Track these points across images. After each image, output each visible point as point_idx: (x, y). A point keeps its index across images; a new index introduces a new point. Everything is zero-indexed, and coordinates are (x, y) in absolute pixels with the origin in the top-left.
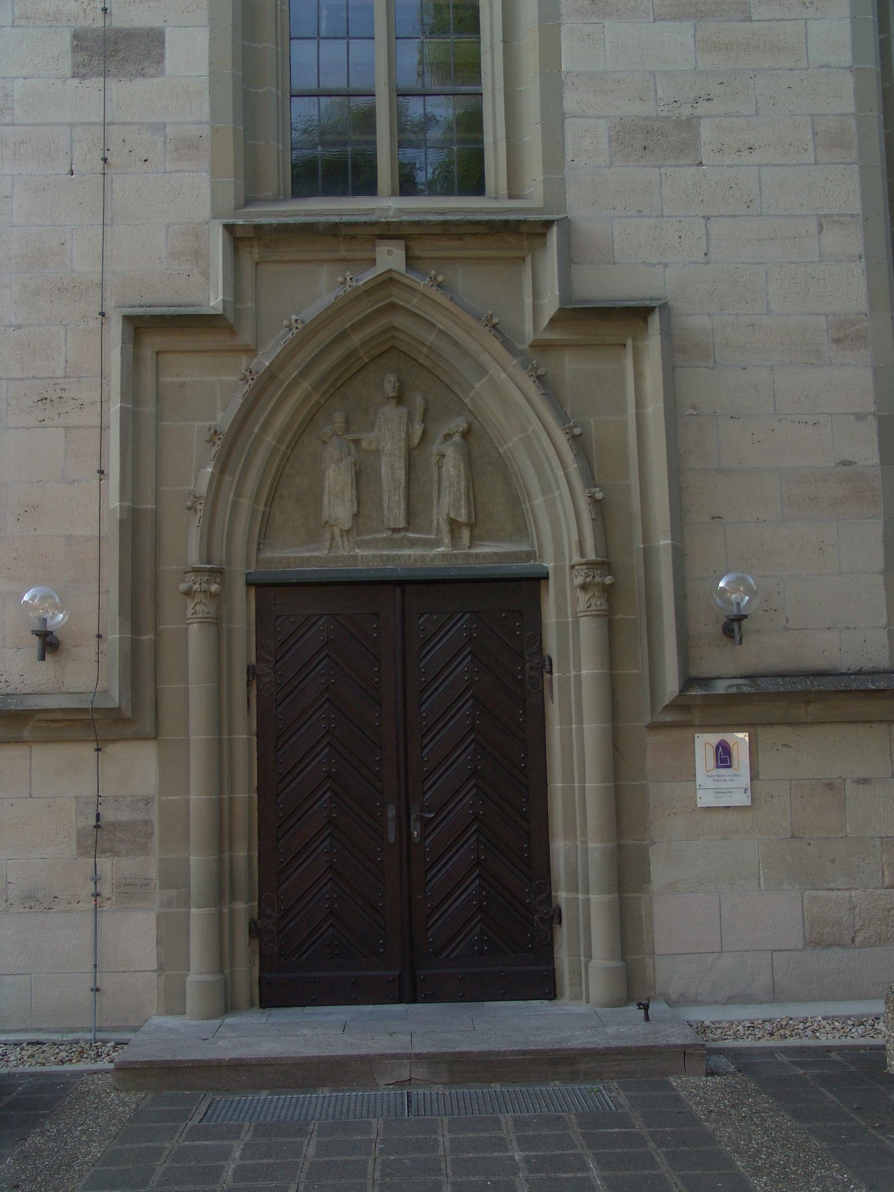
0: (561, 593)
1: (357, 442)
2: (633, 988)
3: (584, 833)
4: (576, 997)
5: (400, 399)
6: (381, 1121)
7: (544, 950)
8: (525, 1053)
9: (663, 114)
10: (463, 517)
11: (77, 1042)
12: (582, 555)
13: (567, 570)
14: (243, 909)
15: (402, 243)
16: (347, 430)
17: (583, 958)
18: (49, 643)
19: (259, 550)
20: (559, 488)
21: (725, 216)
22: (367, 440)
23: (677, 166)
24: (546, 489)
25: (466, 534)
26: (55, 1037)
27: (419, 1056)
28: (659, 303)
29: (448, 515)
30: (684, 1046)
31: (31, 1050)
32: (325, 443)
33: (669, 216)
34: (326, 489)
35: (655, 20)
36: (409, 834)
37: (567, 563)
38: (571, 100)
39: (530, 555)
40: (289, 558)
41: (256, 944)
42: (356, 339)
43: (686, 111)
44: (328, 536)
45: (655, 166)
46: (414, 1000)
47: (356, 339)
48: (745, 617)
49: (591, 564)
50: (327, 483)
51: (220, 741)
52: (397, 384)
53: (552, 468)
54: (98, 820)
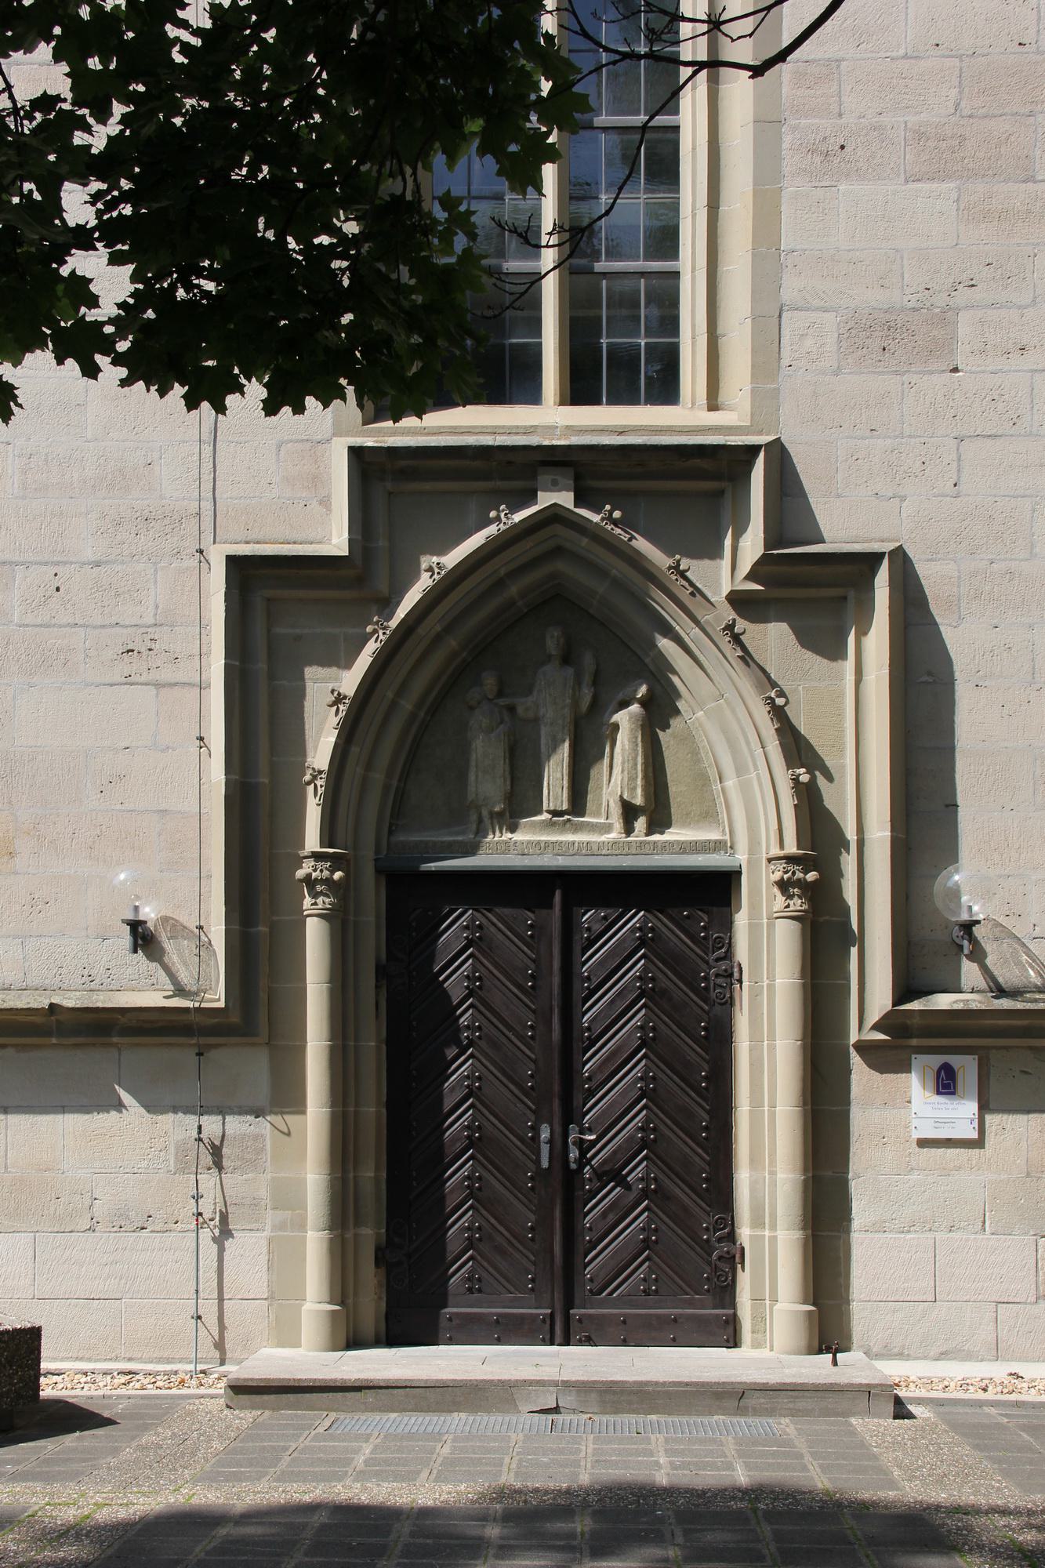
0: (755, 892)
1: (512, 709)
2: (828, 1331)
3: (773, 1162)
4: (757, 1345)
5: (567, 659)
6: (521, 1435)
7: (726, 1293)
8: (687, 1384)
9: (911, 305)
10: (638, 800)
11: (176, 1373)
12: (782, 847)
13: (764, 861)
14: (370, 1234)
15: (571, 471)
16: (500, 694)
17: (768, 1302)
18: (142, 938)
19: (390, 833)
20: (756, 768)
21: (984, 436)
22: (524, 706)
23: (924, 373)
24: (740, 770)
25: (641, 824)
26: (150, 1367)
27: (567, 1384)
28: (887, 547)
29: (621, 796)
30: (868, 1385)
31: (123, 1379)
32: (472, 708)
33: (910, 436)
34: (473, 763)
35: (906, 181)
36: (567, 1155)
37: (764, 856)
38: (791, 288)
39: (717, 846)
40: (427, 843)
41: (383, 1271)
42: (513, 590)
43: (941, 300)
44: (474, 817)
45: (896, 373)
46: (567, 1342)
47: (513, 590)
48: (978, 922)
49: (790, 859)
50: (474, 756)
51: (345, 1047)
52: (562, 640)
53: (748, 743)
54: (200, 1132)
